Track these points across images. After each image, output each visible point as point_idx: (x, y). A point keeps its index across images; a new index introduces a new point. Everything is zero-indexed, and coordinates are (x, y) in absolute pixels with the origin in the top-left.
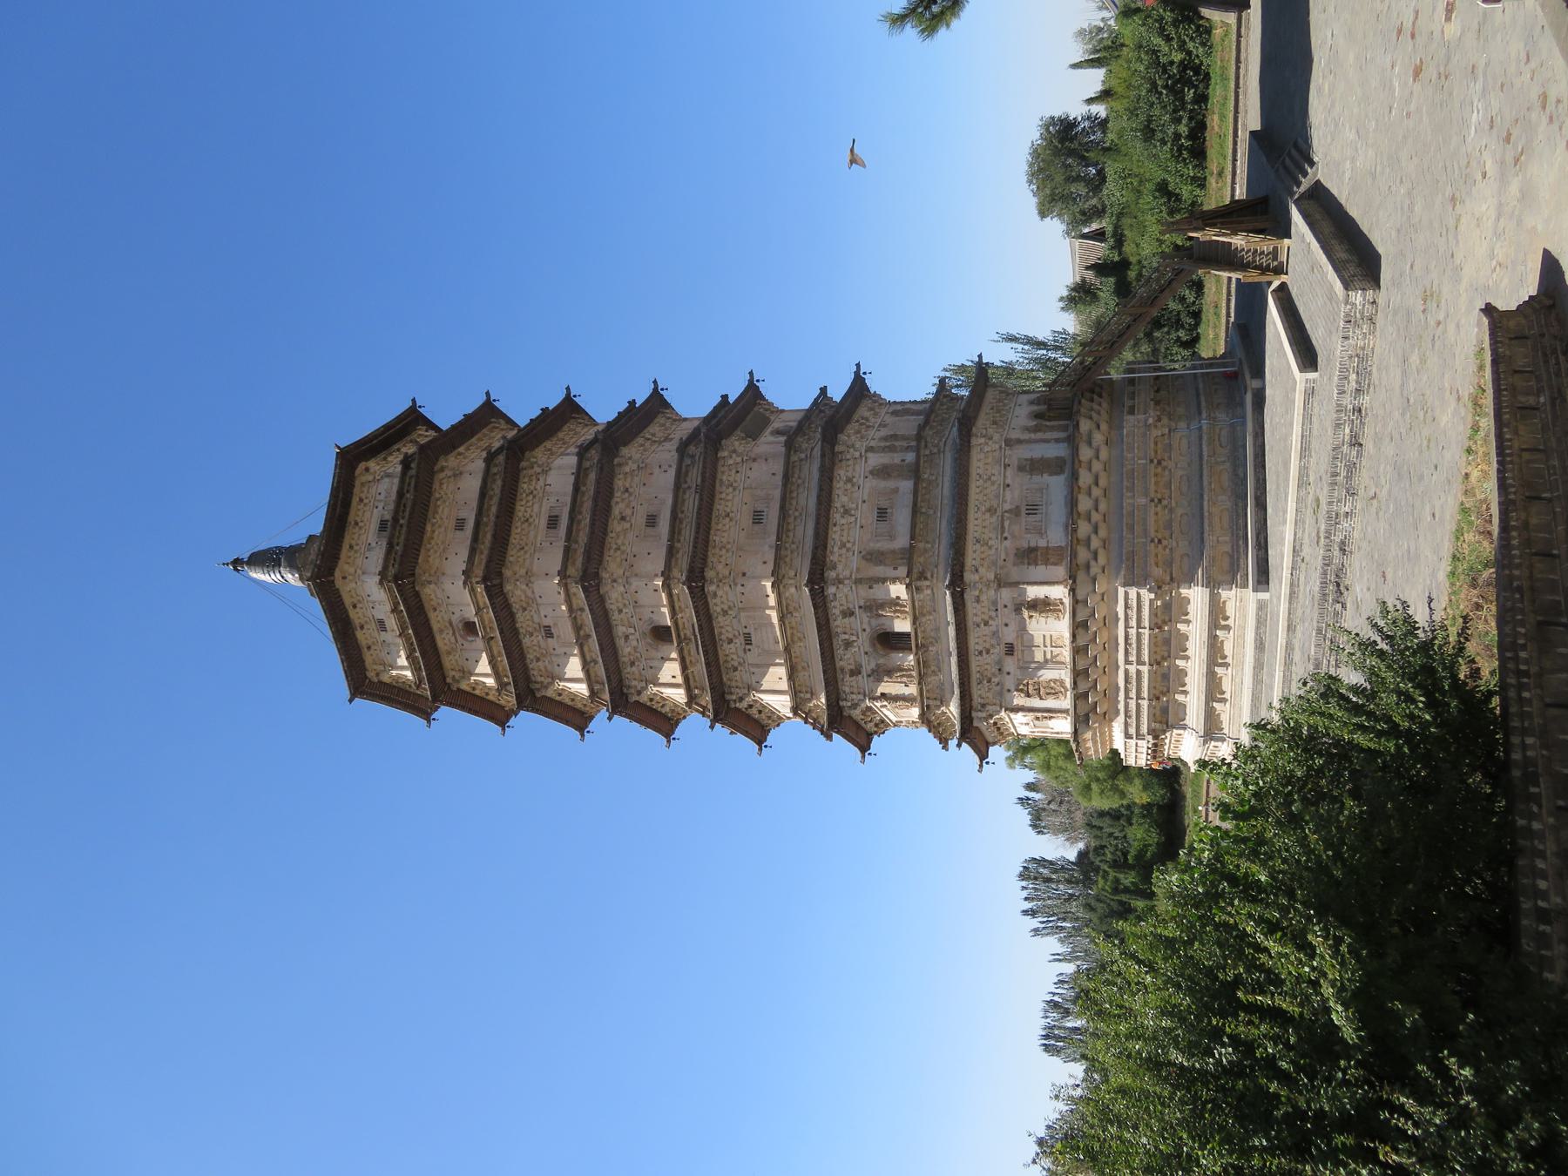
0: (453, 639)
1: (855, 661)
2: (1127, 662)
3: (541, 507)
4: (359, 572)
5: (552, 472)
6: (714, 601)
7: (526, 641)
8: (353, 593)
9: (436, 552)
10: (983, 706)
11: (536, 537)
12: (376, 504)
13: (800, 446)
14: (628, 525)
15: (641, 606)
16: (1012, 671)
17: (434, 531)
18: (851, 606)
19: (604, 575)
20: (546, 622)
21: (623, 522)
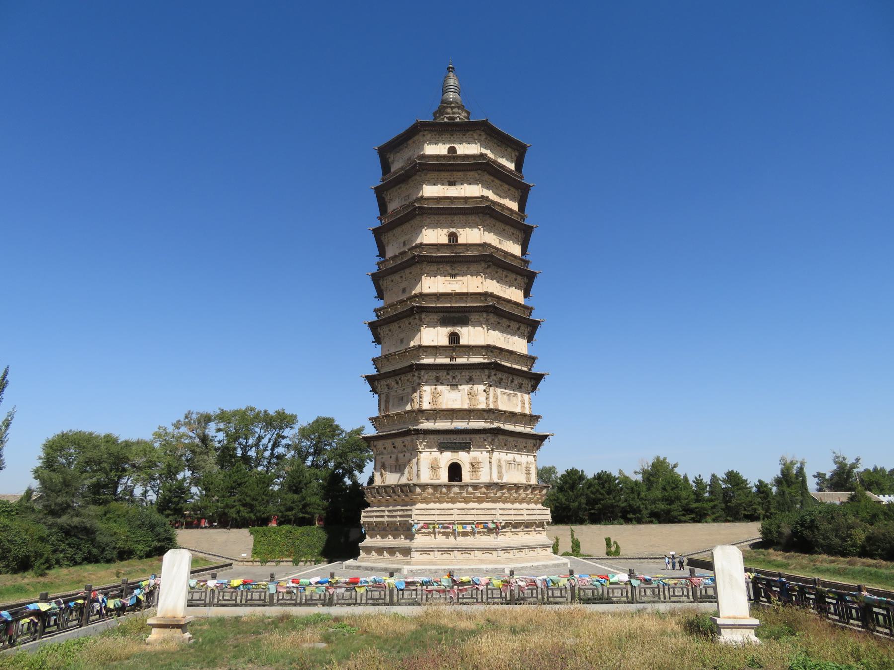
2: (389, 511)
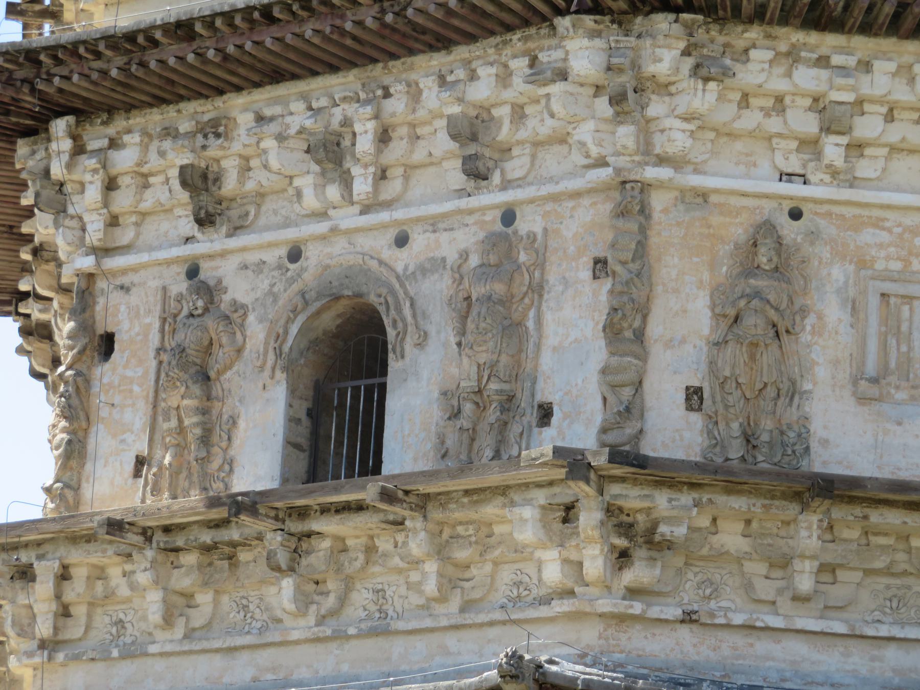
1: (261, 196)
18: (516, 167)
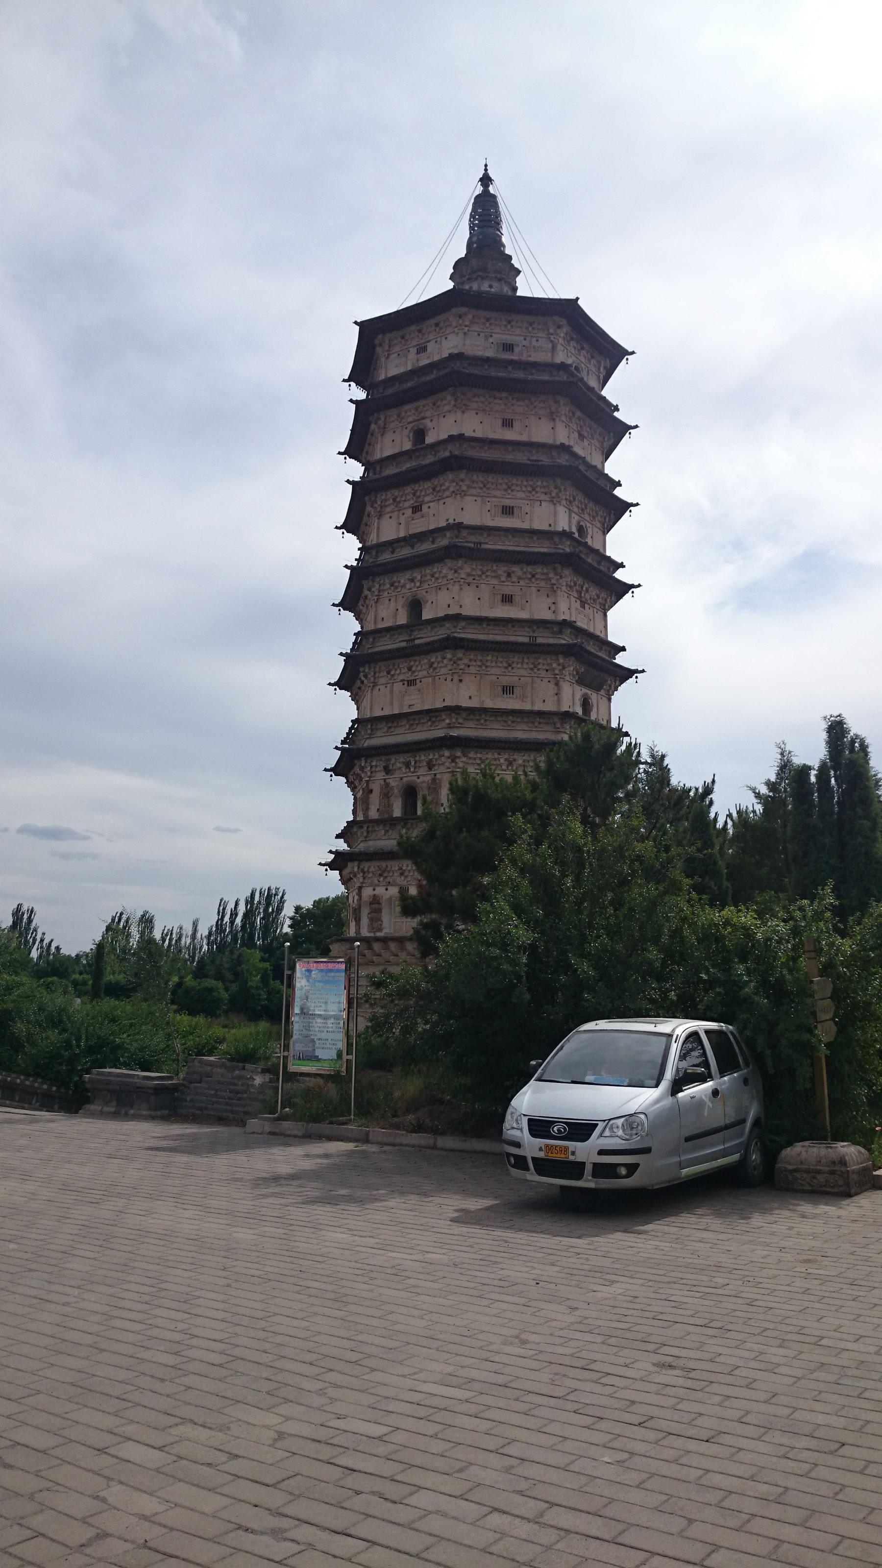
0: (410, 419)
3: (521, 499)
4: (466, 329)
5: (552, 507)
6: (439, 657)
7: (408, 490)
8: (447, 323)
9: (483, 402)
10: (363, 871)
11: (494, 497)
12: (528, 339)
13: (566, 723)
14: (503, 579)
15: (436, 591)
16: (388, 892)
17: (501, 399)
19: (460, 563)
20: (425, 508)
21: (506, 574)
